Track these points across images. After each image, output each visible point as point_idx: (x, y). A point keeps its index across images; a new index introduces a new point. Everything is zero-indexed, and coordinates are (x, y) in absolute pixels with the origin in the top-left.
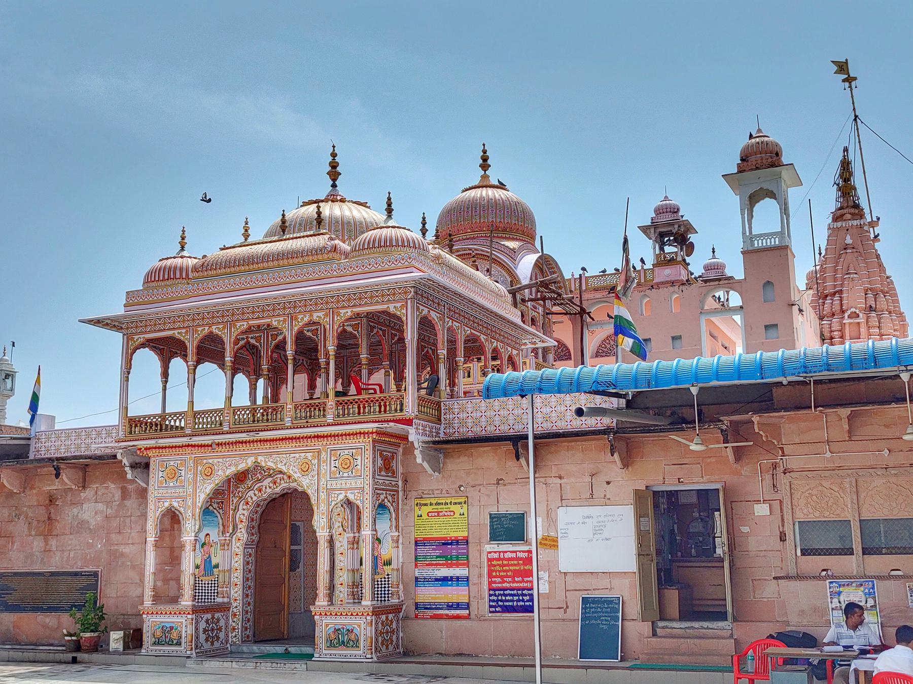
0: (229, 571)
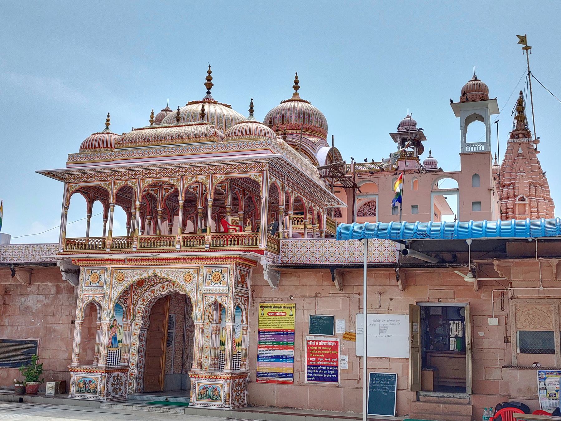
0: (129, 345)
